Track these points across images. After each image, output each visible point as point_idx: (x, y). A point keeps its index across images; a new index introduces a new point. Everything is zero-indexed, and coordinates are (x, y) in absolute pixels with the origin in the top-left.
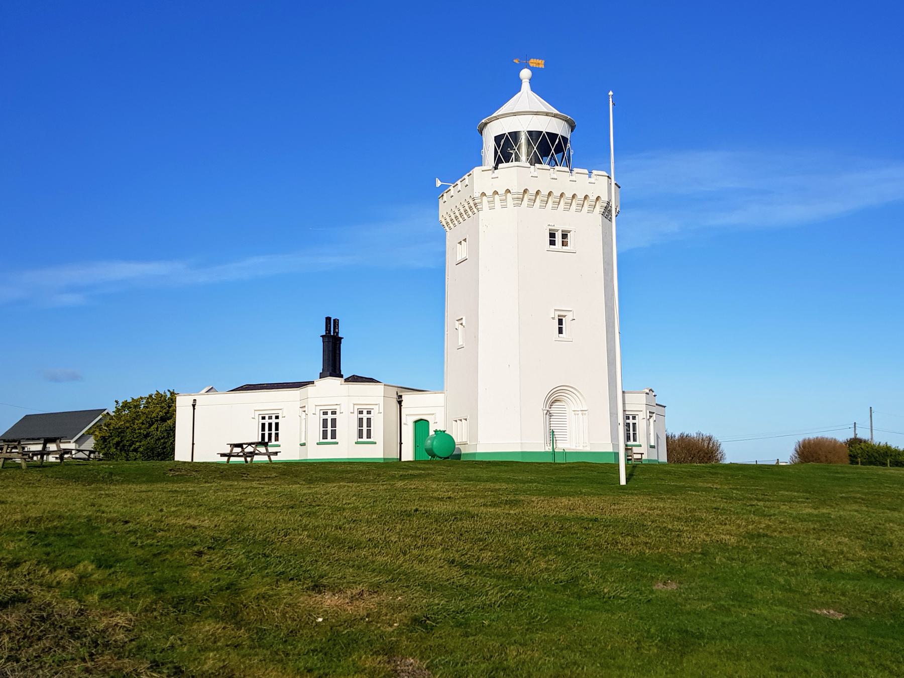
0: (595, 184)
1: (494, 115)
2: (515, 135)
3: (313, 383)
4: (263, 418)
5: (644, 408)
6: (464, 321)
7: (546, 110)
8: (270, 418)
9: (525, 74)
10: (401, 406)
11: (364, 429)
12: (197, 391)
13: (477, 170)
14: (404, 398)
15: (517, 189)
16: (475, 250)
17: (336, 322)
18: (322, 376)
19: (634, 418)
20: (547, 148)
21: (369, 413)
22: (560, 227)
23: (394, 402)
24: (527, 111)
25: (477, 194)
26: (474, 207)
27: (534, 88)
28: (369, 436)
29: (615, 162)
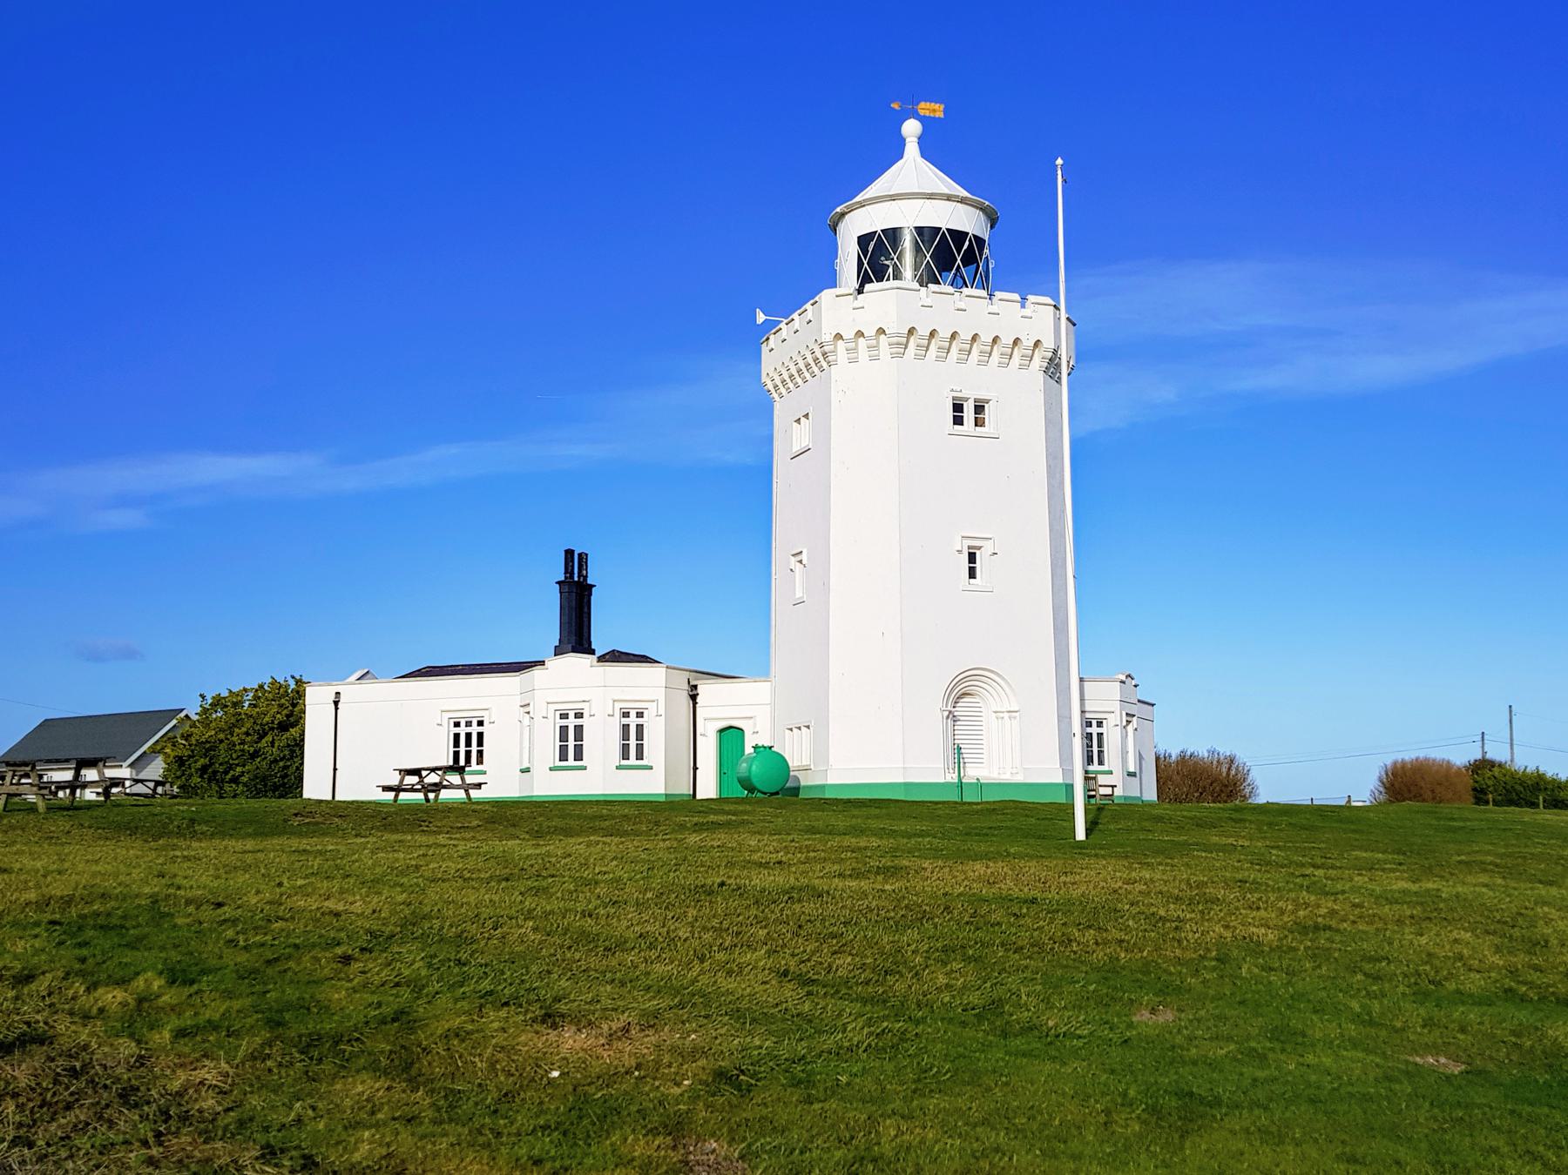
0: (1036, 320)
1: (858, 199)
2: (893, 234)
3: (542, 663)
4: (457, 725)
5: (1116, 706)
6: (804, 557)
7: (946, 191)
8: (469, 724)
9: (911, 128)
10: (695, 703)
11: (632, 744)
12: (342, 678)
13: (826, 296)
14: (700, 689)
15: (896, 327)
16: (823, 433)
17: (583, 558)
18: (558, 651)
19: (1100, 724)
20: (949, 256)
21: (640, 715)
22: (971, 394)
23: (683, 698)
24: (913, 192)
25: (827, 337)
26: (822, 358)
27: (926, 153)
28: (640, 756)
29: (1066, 281)
